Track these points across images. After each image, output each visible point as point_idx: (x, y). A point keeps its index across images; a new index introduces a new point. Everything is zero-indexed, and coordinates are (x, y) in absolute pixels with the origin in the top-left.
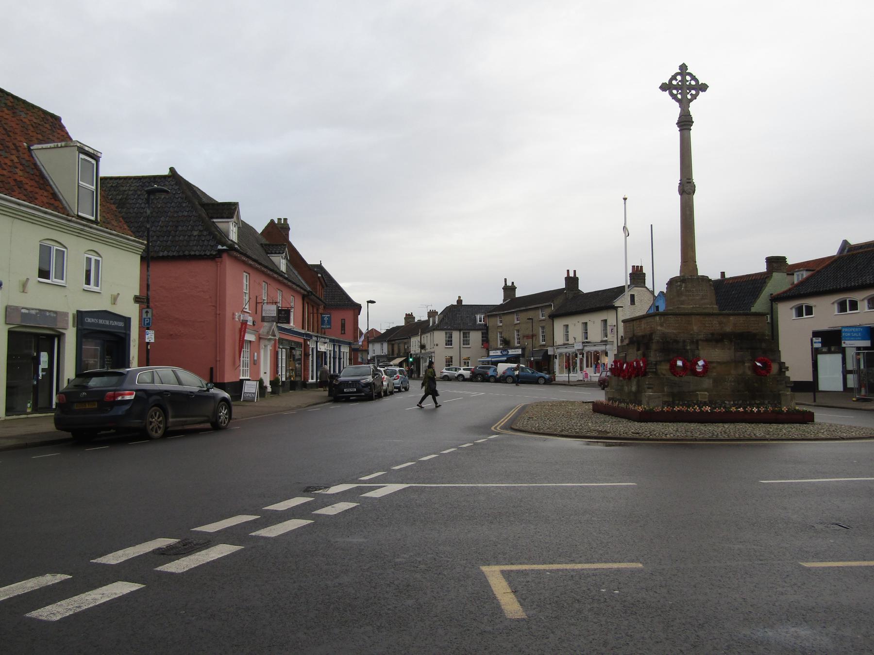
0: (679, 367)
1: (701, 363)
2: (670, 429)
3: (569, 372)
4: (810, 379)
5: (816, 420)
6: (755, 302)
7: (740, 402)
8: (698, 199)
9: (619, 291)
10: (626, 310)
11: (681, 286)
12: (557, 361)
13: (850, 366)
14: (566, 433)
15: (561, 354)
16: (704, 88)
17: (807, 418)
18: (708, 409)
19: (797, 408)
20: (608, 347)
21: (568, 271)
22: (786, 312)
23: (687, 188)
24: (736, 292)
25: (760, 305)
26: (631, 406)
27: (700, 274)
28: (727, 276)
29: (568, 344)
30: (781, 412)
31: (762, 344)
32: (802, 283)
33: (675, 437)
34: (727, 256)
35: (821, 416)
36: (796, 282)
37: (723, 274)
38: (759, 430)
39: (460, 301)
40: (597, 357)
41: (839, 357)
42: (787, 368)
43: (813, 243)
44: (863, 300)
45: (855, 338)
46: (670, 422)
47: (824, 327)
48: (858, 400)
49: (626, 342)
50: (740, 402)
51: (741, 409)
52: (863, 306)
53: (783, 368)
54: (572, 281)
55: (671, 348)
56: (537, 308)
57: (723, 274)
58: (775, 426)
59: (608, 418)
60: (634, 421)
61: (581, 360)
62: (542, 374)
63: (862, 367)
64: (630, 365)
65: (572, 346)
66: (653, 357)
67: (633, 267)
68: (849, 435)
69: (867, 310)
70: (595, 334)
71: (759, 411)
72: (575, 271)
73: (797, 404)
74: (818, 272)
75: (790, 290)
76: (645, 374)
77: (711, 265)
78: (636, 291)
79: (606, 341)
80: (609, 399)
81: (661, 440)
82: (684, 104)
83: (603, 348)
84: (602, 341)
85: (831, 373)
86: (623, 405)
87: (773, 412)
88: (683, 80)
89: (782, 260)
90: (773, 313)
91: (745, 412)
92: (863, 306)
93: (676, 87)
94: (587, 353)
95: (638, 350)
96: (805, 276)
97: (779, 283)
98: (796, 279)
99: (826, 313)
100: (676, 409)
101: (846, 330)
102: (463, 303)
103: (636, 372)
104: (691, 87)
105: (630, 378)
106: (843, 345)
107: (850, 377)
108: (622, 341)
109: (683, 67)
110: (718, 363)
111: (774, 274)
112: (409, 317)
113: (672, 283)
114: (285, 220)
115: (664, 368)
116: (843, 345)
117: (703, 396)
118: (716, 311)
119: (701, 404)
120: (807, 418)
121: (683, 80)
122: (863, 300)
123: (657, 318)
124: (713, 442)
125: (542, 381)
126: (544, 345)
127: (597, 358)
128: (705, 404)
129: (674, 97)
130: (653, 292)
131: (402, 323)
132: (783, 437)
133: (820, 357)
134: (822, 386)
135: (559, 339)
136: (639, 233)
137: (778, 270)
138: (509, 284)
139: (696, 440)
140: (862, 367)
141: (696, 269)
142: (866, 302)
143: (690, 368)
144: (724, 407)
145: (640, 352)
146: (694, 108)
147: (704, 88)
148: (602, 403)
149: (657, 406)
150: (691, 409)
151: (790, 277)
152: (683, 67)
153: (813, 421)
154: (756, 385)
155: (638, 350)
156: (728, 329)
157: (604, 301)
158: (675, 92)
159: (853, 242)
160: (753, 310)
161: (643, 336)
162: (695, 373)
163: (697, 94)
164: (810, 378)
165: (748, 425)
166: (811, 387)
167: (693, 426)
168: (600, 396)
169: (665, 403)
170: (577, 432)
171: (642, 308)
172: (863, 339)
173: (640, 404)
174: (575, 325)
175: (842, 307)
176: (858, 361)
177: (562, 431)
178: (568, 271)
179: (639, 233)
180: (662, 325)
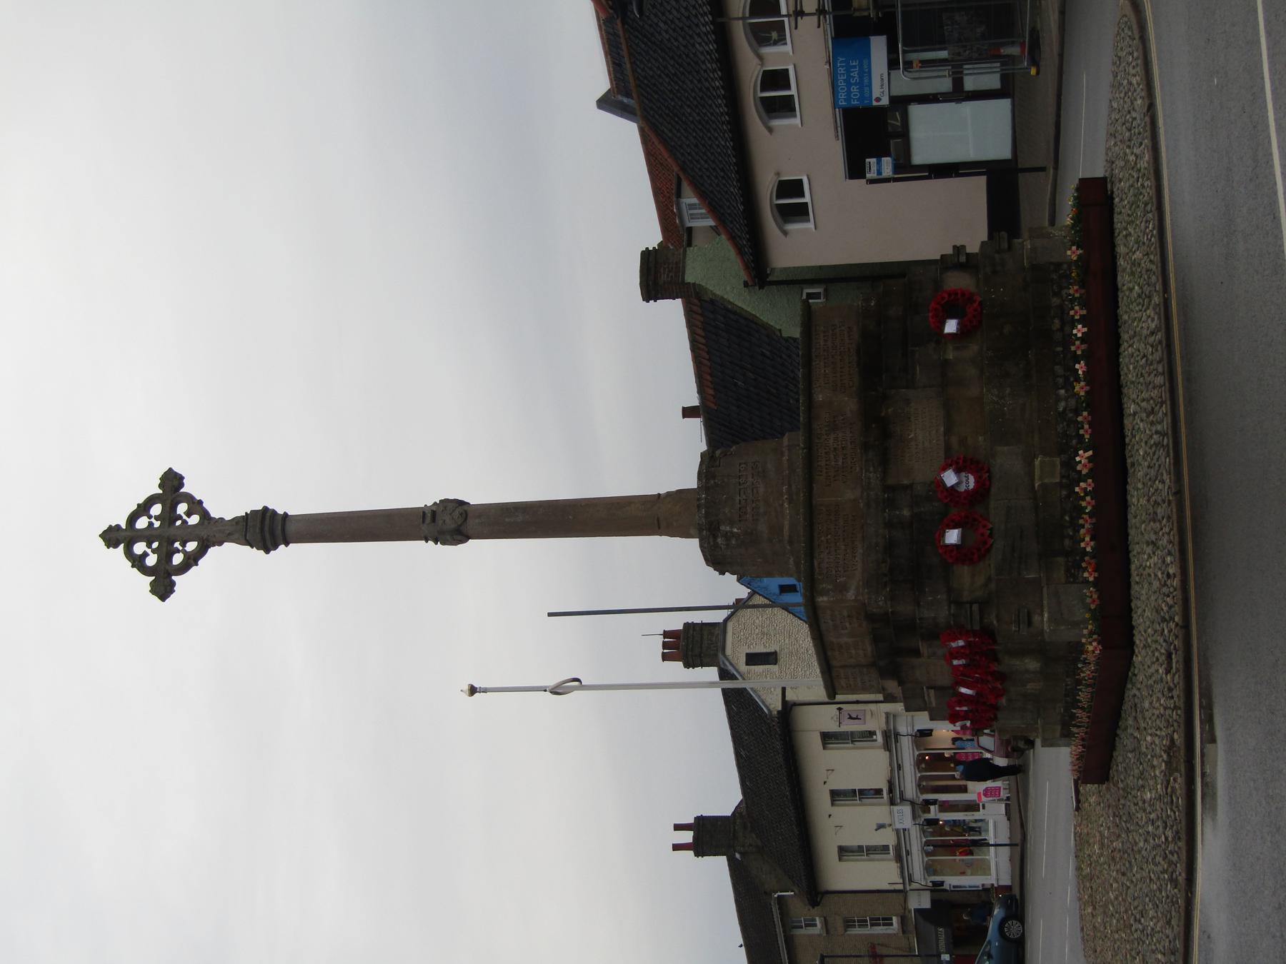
0: (963, 537)
1: (950, 478)
2: (1151, 562)
3: (984, 844)
4: (982, 181)
5: (1099, 173)
6: (765, 327)
7: (1059, 370)
8: (481, 491)
9: (739, 705)
10: (796, 678)
11: (728, 536)
12: (951, 881)
13: (945, 85)
14: (1180, 869)
15: (929, 869)
17: (1096, 196)
18: (1083, 457)
19: (1069, 221)
20: (903, 729)
21: (677, 847)
22: (794, 248)
23: (450, 523)
24: (740, 382)
25: (780, 315)
26: (1087, 673)
27: (691, 482)
28: (694, 401)
29: (898, 848)
30: (1083, 262)
31: (891, 300)
32: (714, 208)
33: (1175, 550)
34: (636, 407)
35: (1088, 157)
36: (710, 222)
37: (688, 412)
38: (1139, 321)
40: (932, 762)
41: (916, 111)
42: (958, 249)
43: (608, 185)
44: (760, 57)
45: (866, 73)
46: (1128, 562)
47: (834, 150)
48: (1035, 62)
49: (892, 686)
50: (1059, 370)
51: (1081, 367)
52: (777, 56)
53: (958, 260)
54: (706, 836)
55: (909, 561)
56: (789, 941)
57: (688, 412)
58: (1123, 279)
59: (1125, 741)
60: (1129, 663)
61: (946, 807)
62: (992, 926)
63: (943, 54)
64: (961, 677)
65: (901, 834)
66: (937, 611)
67: (665, 657)
68: (1141, 91)
69: (788, 48)
70: (864, 766)
71: (1083, 320)
72: (678, 827)
73: (1052, 222)
74: (683, 169)
75: (732, 238)
76: (988, 634)
77: (671, 456)
78: (736, 651)
79: (886, 735)
80: (1067, 735)
81: (1184, 582)
83: (906, 744)
84: (887, 747)
85: (962, 129)
86: (1084, 696)
87: (1083, 284)
88: (148, 536)
89: (650, 262)
90: (798, 280)
91: (1087, 356)
92: (777, 56)
93: (166, 554)
94: (923, 790)
95: (917, 653)
96: (695, 200)
97: (714, 264)
98: (703, 222)
99: (799, 146)
100: (1088, 545)
101: (842, 96)
103: (984, 655)
104: (169, 516)
105: (1002, 677)
106: (885, 101)
107: (970, 84)
108: (889, 699)
109: (112, 537)
110: (948, 432)
111: (689, 278)
113: (717, 560)
115: (968, 579)
116: (885, 101)
117: (1046, 471)
118: (800, 437)
119: (1071, 476)
120: (1096, 196)
121: (148, 536)
122: (760, 57)
123: (822, 600)
124: (1183, 443)
125: (1013, 929)
126: (903, 920)
127: (937, 761)
128: (1070, 464)
129: (192, 560)
130: (739, 605)
132: (1157, 259)
133: (918, 158)
134: (999, 148)
135: (882, 874)
136: (567, 650)
137: (679, 268)
139: (1179, 493)
140: (943, 54)
142: (767, 50)
143: (965, 509)
144: (1077, 412)
145: (924, 648)
146: (224, 507)
148: (1080, 757)
149: (1081, 600)
150: (1087, 504)
151: (698, 240)
152: (112, 537)
153: (1103, 181)
154: (1007, 329)
155: (917, 653)
156: (849, 405)
157: (765, 741)
158: (178, 559)
159: (601, 82)
160: (796, 333)
161: (876, 639)
162: (981, 494)
163: (189, 499)
164: (977, 187)
165: (1127, 351)
166: (1002, 180)
167: (1137, 500)
168: (1055, 766)
169: (1072, 575)
170: (1177, 836)
171: (789, 634)
172: (868, 55)
173: (1078, 648)
174: (838, 826)
175: (784, 107)
176: (926, 63)
177: (1174, 882)
178: (677, 847)
179: (567, 650)
180: (843, 588)
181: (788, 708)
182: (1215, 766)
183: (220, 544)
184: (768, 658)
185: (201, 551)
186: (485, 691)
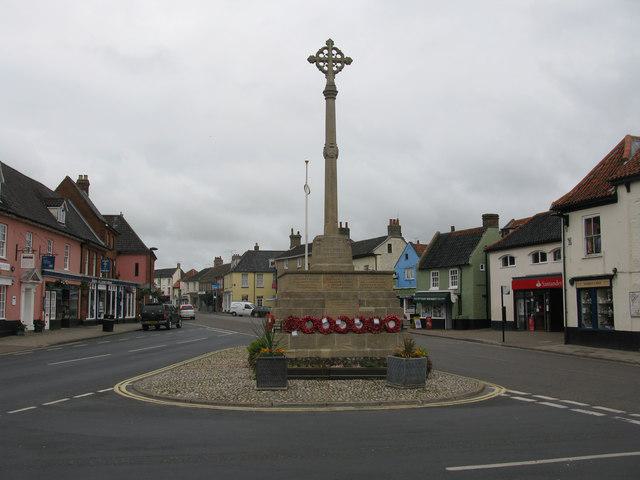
22: (495, 260)
23: (331, 153)
25: (476, 256)
37: (453, 228)
39: (257, 247)
57: (453, 228)
78: (392, 241)
82: (330, 75)
90: (487, 262)
93: (336, 61)
97: (491, 237)
104: (336, 61)
112: (218, 260)
129: (321, 68)
131: (212, 265)
138: (295, 233)
146: (339, 80)
175: (536, 260)
181: (375, 256)
184: (390, 250)
185: (324, 72)
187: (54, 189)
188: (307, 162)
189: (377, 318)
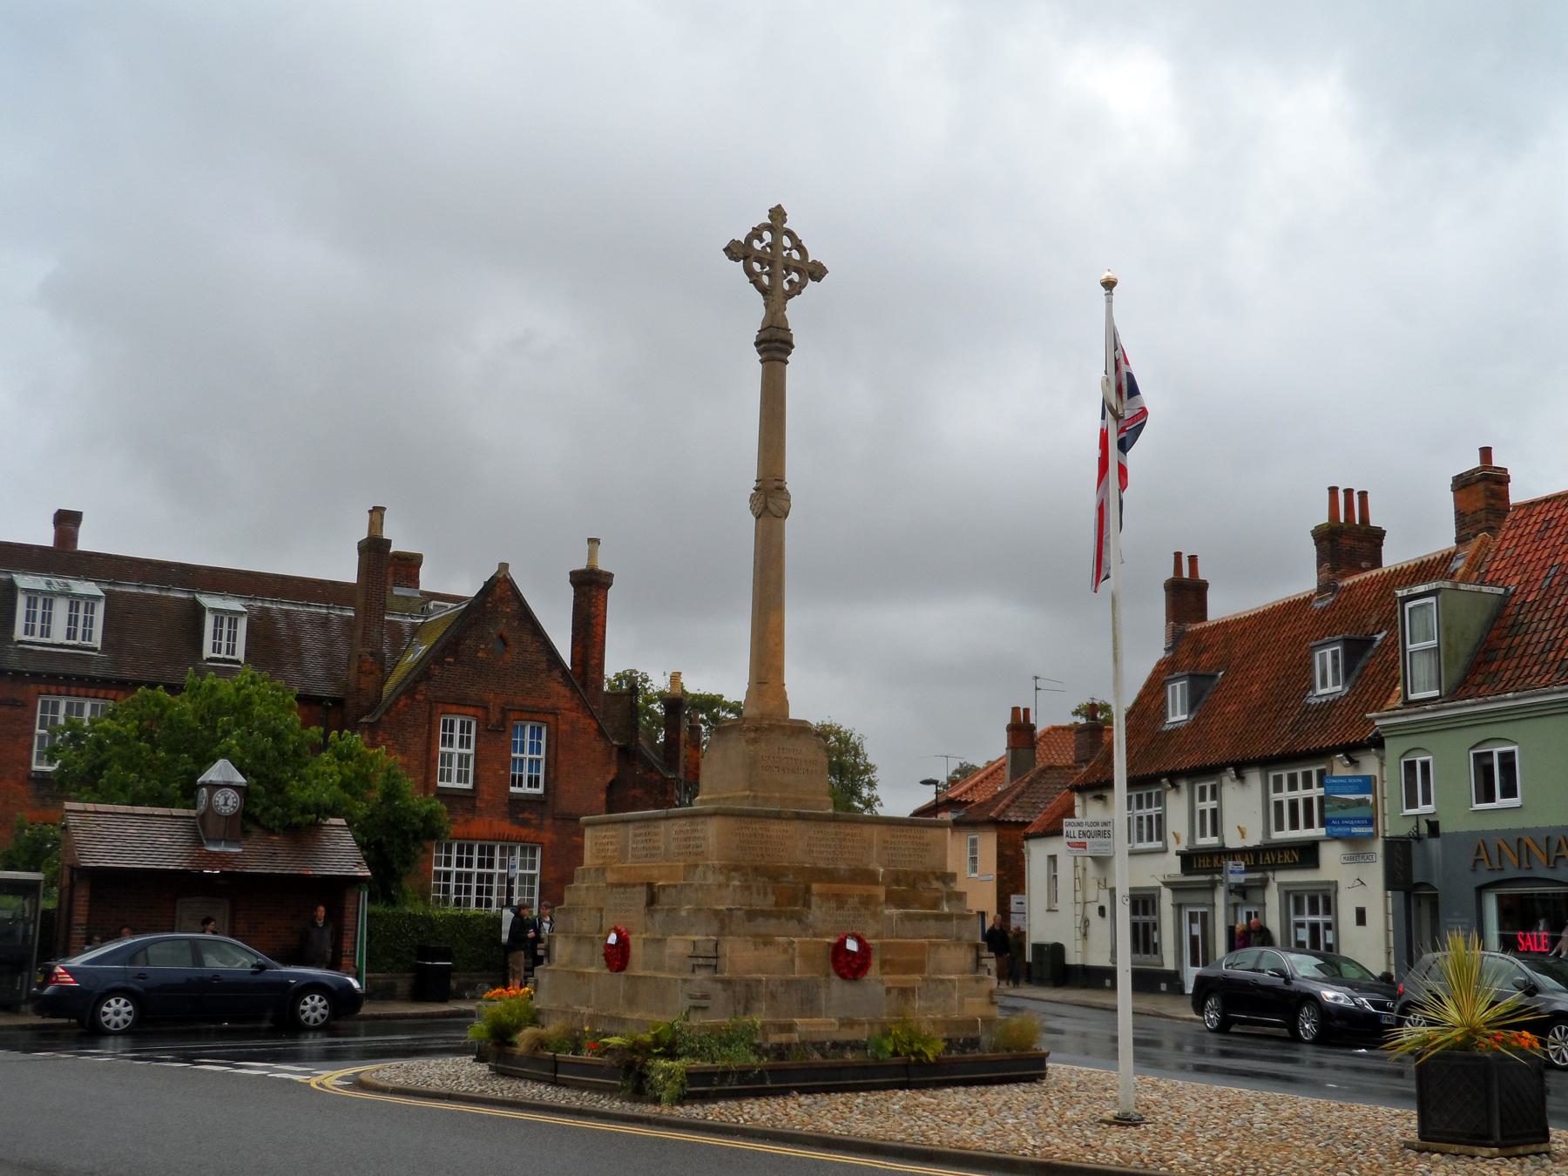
16: (816, 272)
27: (793, 715)
57: (675, 678)
102: (1520, 492)
109: (778, 214)
114: (1026, 711)
129: (754, 279)
141: (784, 704)
146: (795, 312)
147: (816, 272)
152: (778, 214)
182: (1273, 1048)
183: (766, 305)
185: (764, 291)
186: (1109, 302)
187: (792, 716)
188: (1109, 285)
189: (859, 940)
